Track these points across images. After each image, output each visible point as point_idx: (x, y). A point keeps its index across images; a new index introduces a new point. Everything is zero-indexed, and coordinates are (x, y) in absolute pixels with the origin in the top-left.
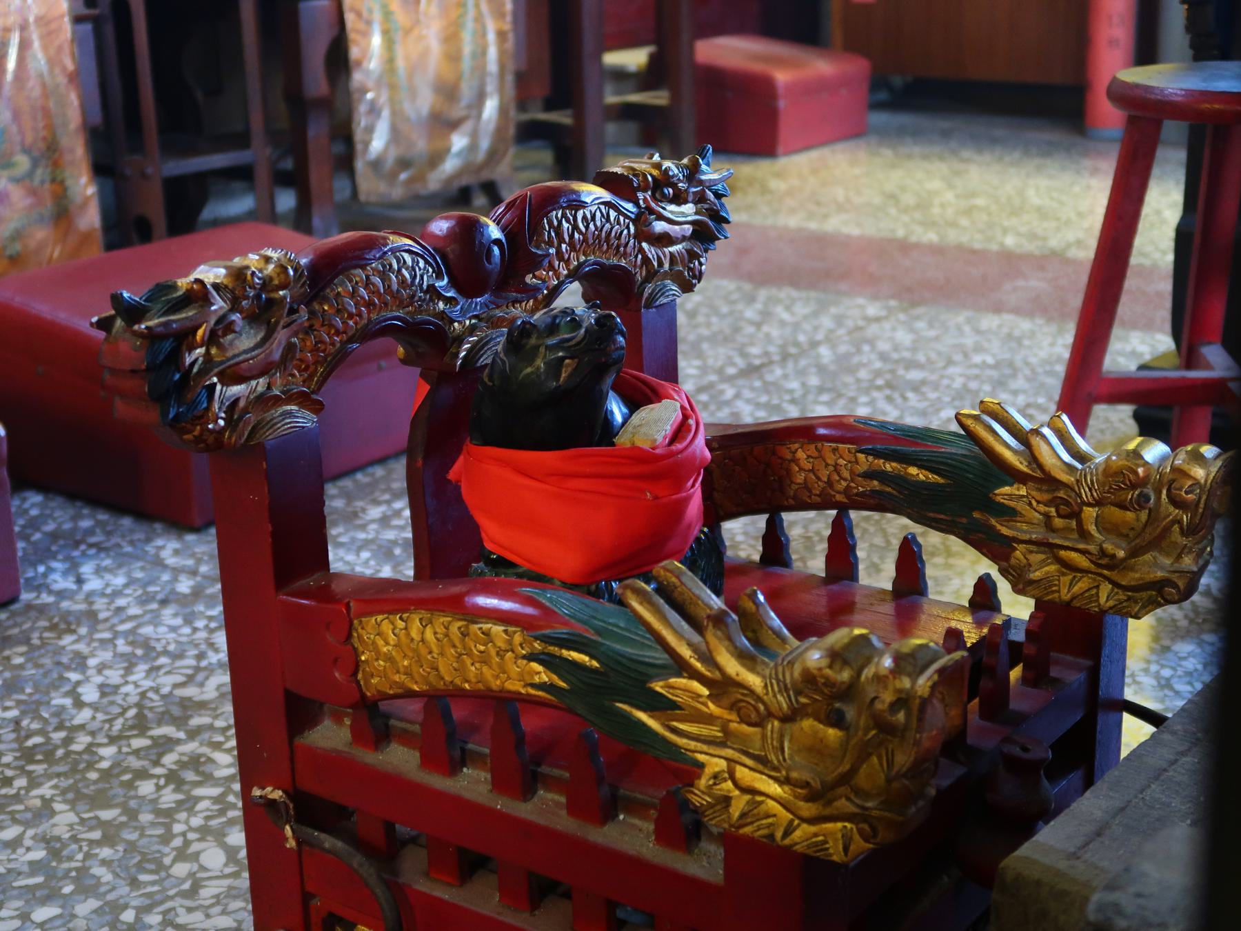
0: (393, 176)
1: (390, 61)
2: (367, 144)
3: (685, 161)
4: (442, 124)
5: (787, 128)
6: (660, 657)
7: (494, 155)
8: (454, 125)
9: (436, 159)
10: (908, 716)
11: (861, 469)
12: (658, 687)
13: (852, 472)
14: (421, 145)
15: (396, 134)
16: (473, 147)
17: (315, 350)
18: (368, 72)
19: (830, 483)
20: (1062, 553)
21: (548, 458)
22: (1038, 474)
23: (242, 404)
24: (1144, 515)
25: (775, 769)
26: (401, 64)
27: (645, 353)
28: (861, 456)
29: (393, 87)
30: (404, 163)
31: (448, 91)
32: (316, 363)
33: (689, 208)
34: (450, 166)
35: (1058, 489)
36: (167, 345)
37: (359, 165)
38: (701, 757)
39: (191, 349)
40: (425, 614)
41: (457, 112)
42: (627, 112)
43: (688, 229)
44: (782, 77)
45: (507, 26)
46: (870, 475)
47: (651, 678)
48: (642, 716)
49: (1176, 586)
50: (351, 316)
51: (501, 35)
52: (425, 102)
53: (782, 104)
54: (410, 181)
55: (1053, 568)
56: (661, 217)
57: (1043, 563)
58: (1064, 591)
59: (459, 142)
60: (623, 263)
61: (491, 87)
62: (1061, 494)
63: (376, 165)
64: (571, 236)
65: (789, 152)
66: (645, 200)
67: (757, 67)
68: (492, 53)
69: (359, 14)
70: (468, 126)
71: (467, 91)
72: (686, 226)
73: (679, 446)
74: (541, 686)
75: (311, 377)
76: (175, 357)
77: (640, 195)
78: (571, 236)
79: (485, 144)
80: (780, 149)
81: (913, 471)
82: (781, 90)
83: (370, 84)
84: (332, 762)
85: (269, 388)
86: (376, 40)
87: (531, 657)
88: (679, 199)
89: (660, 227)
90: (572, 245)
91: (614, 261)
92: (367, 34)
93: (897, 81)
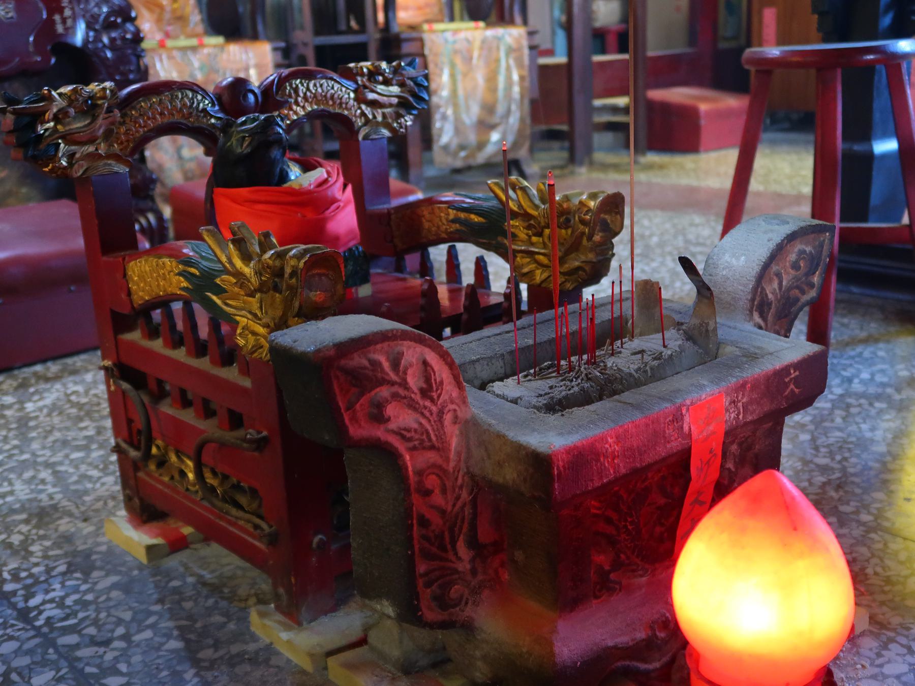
0: (455, 155)
1: (454, 92)
2: (440, 136)
3: (394, 64)
4: (485, 126)
5: (706, 136)
6: (218, 267)
7: (516, 145)
8: (493, 127)
9: (481, 146)
10: (297, 280)
11: (451, 217)
12: (218, 281)
13: (447, 219)
14: (472, 138)
15: (457, 131)
16: (503, 138)
17: (126, 133)
18: (441, 97)
19: (438, 227)
20: (537, 257)
21: (244, 192)
22: (522, 212)
23: (77, 156)
24: (570, 231)
25: (260, 319)
26: (461, 92)
27: (363, 164)
28: (450, 211)
29: (456, 106)
30: (462, 147)
31: (489, 108)
32: (128, 141)
33: (395, 89)
34: (490, 150)
35: (530, 220)
36: (26, 120)
37: (436, 148)
38: (238, 318)
39: (43, 122)
40: (146, 257)
41: (496, 119)
42: (611, 127)
43: (395, 101)
44: (703, 107)
45: (525, 73)
46: (454, 221)
47: (217, 277)
48: (214, 298)
49: (584, 271)
50: (149, 118)
51: (522, 78)
52: (473, 113)
53: (703, 122)
54: (466, 157)
55: (533, 266)
56: (373, 91)
57: (529, 263)
58: (538, 278)
59: (495, 136)
60: (346, 112)
61: (514, 107)
62: (532, 222)
63: (446, 148)
64: (305, 94)
65: (708, 149)
66: (362, 81)
67: (688, 102)
68: (516, 89)
69: (436, 65)
70: (501, 128)
71: (500, 109)
72: (393, 99)
73: (320, 189)
74: (184, 289)
75: (126, 148)
76: (32, 126)
77: (359, 79)
78: (305, 94)
79: (510, 139)
80: (702, 148)
81: (473, 216)
82: (702, 114)
83: (442, 103)
84: (132, 345)
85: (97, 149)
86: (445, 77)
87: (180, 274)
88: (387, 82)
89: (371, 96)
90: (305, 98)
91: (338, 111)
92: (440, 76)
93: (795, 116)
